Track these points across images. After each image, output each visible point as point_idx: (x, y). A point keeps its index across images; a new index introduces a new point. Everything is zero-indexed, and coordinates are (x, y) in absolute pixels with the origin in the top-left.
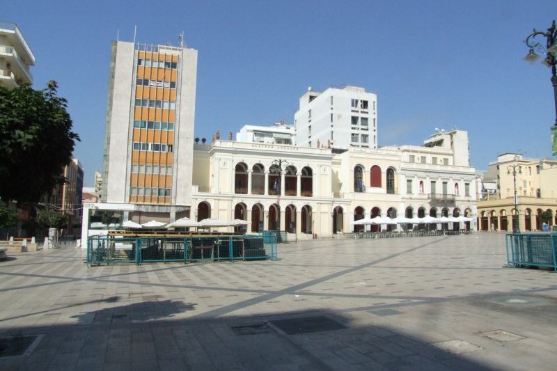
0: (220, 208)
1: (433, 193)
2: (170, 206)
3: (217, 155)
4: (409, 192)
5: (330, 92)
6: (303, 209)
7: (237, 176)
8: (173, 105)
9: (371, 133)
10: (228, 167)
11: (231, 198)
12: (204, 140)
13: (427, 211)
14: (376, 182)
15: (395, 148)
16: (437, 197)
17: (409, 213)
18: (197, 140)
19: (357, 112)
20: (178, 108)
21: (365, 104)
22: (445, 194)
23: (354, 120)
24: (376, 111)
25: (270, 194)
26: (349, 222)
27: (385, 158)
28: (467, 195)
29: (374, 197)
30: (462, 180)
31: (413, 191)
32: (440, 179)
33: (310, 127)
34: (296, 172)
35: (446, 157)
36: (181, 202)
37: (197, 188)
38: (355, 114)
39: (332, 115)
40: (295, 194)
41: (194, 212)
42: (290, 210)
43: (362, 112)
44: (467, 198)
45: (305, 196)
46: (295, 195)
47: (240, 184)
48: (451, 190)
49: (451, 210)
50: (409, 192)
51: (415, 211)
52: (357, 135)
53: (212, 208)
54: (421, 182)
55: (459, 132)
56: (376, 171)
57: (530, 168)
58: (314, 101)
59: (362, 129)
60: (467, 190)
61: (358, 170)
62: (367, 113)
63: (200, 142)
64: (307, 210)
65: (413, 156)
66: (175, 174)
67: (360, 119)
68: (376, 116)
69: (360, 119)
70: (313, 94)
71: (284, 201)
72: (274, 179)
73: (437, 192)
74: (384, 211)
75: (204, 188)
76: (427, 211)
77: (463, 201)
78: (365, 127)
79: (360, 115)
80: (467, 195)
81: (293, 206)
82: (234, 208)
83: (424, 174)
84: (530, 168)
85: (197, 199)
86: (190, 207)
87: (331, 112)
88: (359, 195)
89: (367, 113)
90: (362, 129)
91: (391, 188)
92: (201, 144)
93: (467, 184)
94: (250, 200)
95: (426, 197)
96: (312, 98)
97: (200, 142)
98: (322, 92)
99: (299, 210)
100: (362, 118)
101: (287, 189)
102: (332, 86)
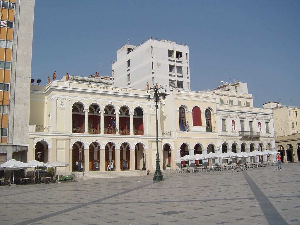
0: (57, 148)
1: (243, 131)
2: (7, 146)
3: (54, 94)
4: (224, 130)
5: (151, 42)
6: (91, 146)
7: (74, 116)
8: (10, 45)
9: (186, 80)
10: (65, 106)
11: (68, 137)
12: (39, 81)
13: (239, 147)
14: (197, 122)
15: (212, 92)
16: (246, 134)
17: (225, 149)
18: (32, 81)
19: (174, 61)
20: (15, 47)
21: (179, 55)
22: (251, 131)
23: (171, 68)
24: (188, 61)
25: (136, 134)
26: (176, 157)
27: (204, 100)
28: (268, 132)
29: (196, 135)
30: (238, 117)
31: (227, 130)
32: (247, 118)
33: (129, 75)
34: (99, 110)
35: (248, 100)
36: (18, 142)
37: (35, 127)
38: (172, 63)
39: (153, 63)
40: (82, 132)
41: (31, 153)
42: (95, 147)
43: (177, 62)
44: (268, 135)
45: (108, 133)
46: (82, 132)
47: (77, 123)
48: (256, 128)
49: (257, 146)
50: (224, 130)
51: (230, 147)
52: (174, 81)
53: (50, 147)
54: (233, 121)
55: (241, 84)
56: (196, 111)
57: (296, 111)
58: (132, 52)
59: (178, 76)
60: (267, 128)
61: (182, 110)
62: (181, 62)
63: (35, 83)
64: (139, 147)
65: (232, 101)
66: (11, 113)
67: (176, 67)
68: (188, 66)
69: (176, 67)
70: (131, 47)
71: (103, 139)
72: (109, 121)
73: (254, 130)
74: (191, 148)
75: (40, 128)
76: (239, 147)
77: (230, 136)
78: (180, 75)
79: (176, 64)
80: (268, 132)
81: (96, 144)
82: (34, 147)
83: (243, 115)
84: (296, 111)
85: (34, 138)
86: (27, 146)
87: (152, 60)
88: (184, 134)
89: (181, 62)
90: (178, 76)
91: (209, 129)
92: (36, 82)
93: (242, 121)
94: (87, 139)
95: (238, 134)
96: (129, 50)
97: (35, 83)
98: (139, 45)
99: (87, 147)
100: (177, 67)
101: (106, 127)
102: (153, 38)
